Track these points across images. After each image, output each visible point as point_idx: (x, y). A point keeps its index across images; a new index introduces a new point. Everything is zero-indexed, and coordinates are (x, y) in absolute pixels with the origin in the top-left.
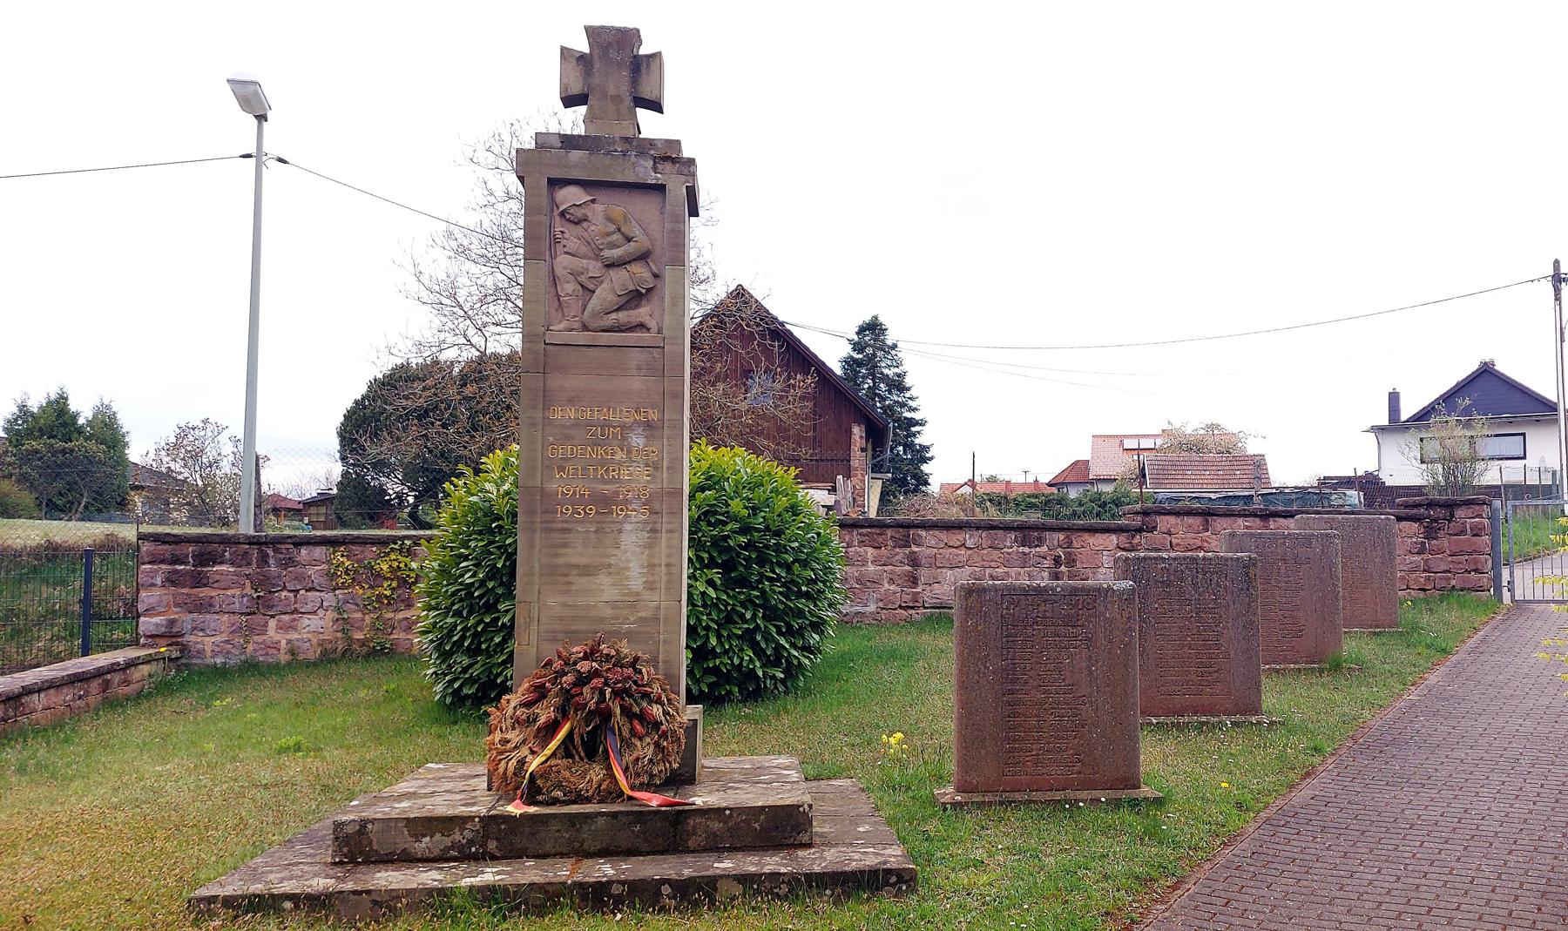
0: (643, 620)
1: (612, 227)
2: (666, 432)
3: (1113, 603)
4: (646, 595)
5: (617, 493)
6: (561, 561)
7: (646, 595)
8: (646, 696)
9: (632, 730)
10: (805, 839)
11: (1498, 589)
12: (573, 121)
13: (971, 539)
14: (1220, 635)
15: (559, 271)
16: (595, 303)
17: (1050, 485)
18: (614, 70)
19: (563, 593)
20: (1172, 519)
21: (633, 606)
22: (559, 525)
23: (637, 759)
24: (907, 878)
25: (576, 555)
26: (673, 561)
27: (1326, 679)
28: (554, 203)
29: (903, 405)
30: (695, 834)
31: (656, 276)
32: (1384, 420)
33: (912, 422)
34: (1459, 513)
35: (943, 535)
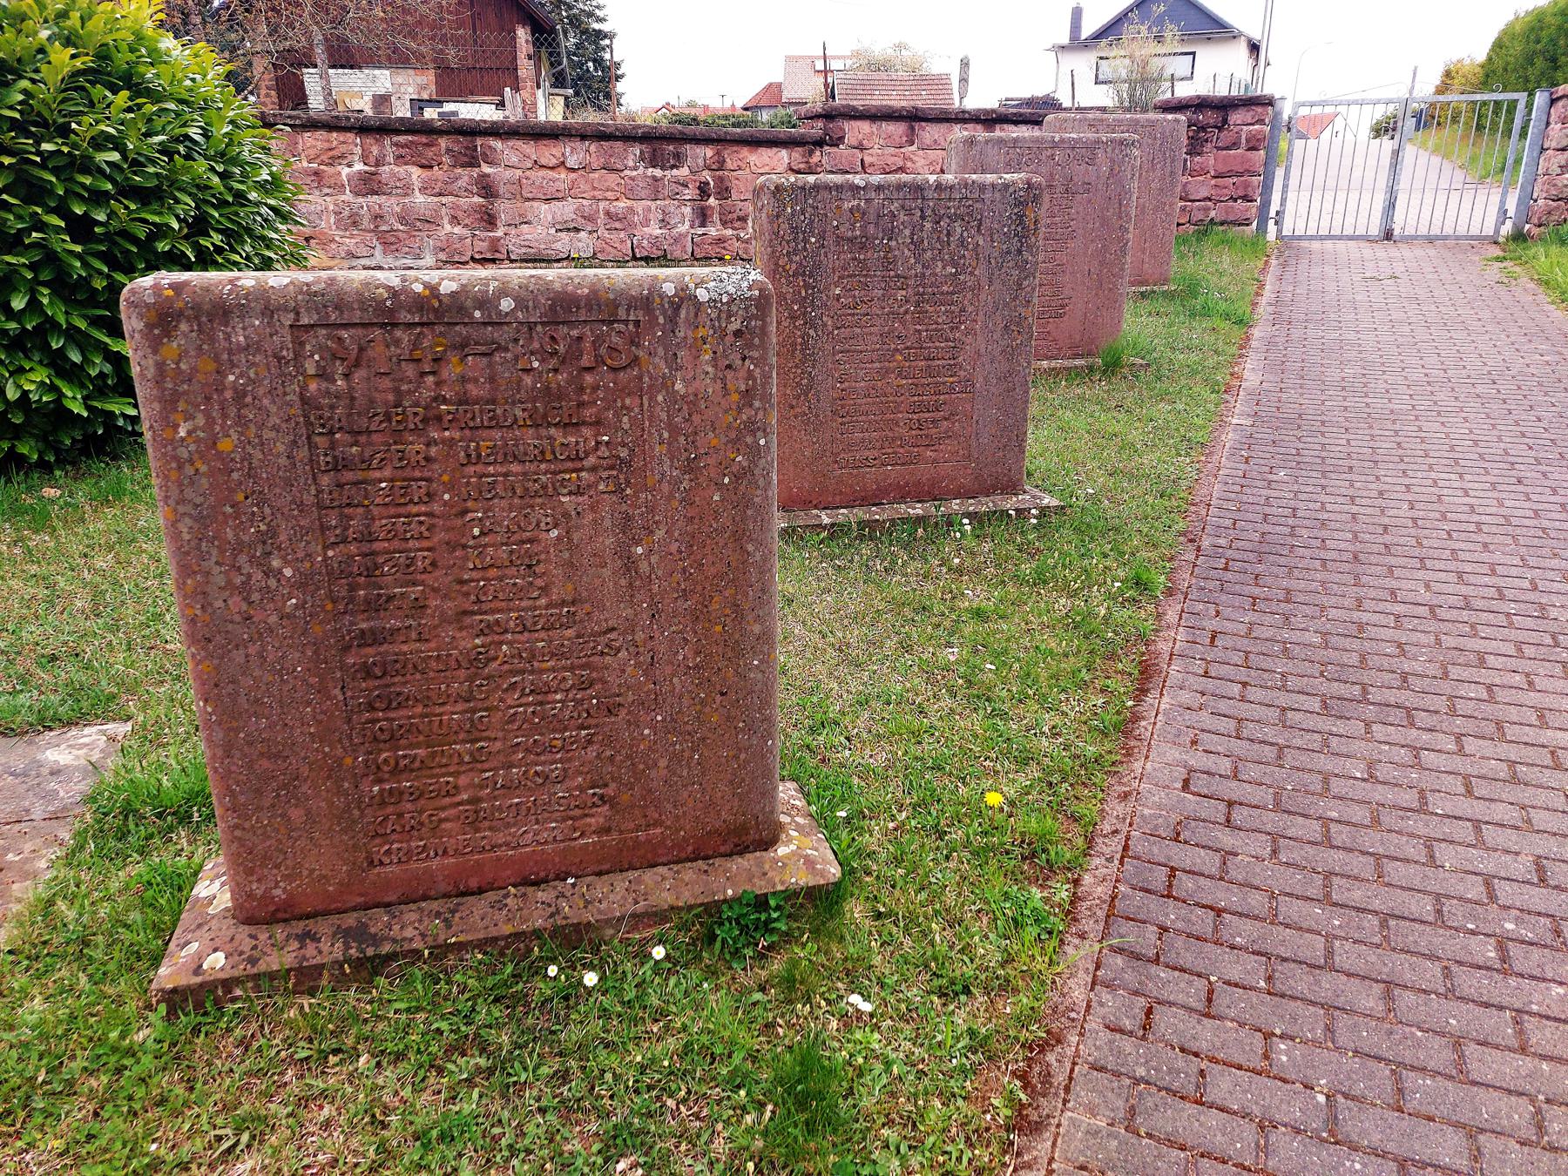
3: (696, 348)
11: (1262, 228)
13: (575, 154)
14: (957, 347)
17: (746, 109)
20: (865, 126)
27: (1100, 388)
29: (590, 15)
32: (1065, 40)
33: (600, 35)
34: (1236, 117)
35: (528, 148)
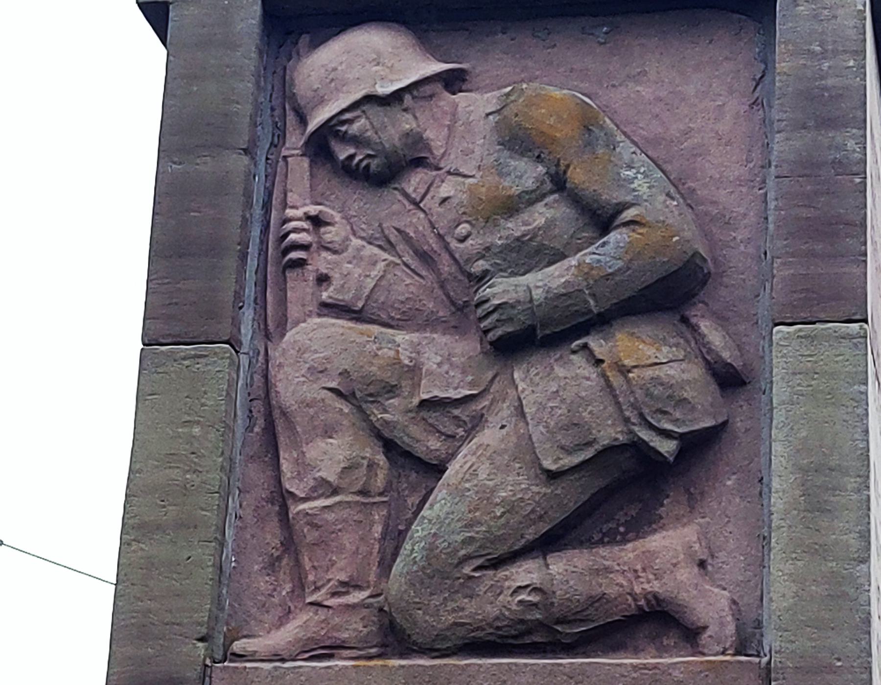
1: (527, 174)
15: (293, 387)
28: (284, 102)
31: (730, 380)
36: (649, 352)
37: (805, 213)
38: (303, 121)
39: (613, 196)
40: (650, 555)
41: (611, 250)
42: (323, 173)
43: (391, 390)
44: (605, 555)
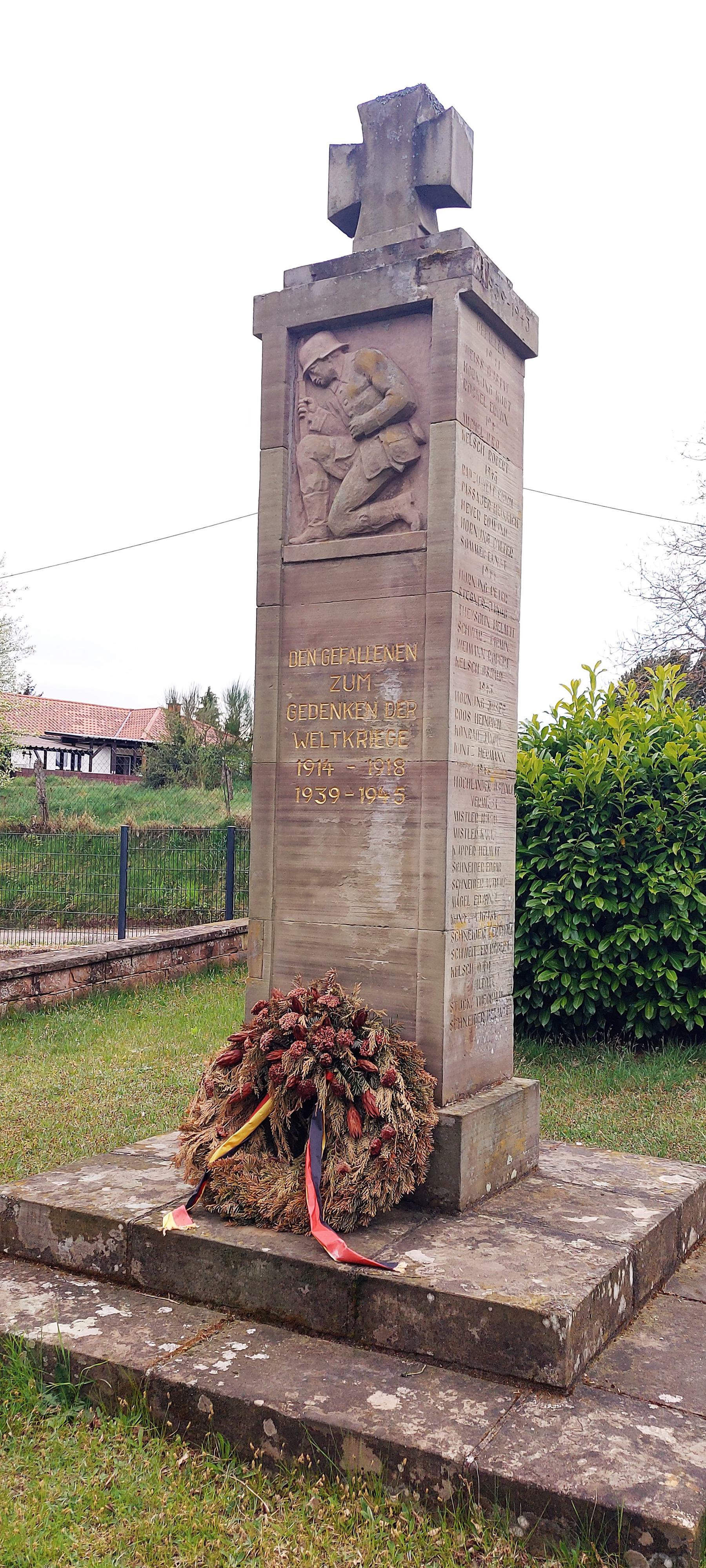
0: (394, 955)
2: (427, 676)
4: (401, 919)
5: (365, 769)
6: (299, 864)
7: (401, 919)
8: (369, 1075)
9: (345, 1124)
10: (552, 1377)
12: (340, 245)
15: (302, 459)
16: (341, 495)
18: (403, 159)
19: (303, 908)
21: (384, 932)
22: (298, 815)
23: (343, 1172)
24: (672, 1544)
25: (317, 857)
26: (434, 870)
30: (383, 1320)
36: (395, 437)
37: (439, 384)
38: (302, 369)
39: (385, 386)
40: (397, 502)
41: (383, 406)
42: (310, 386)
43: (328, 457)
44: (385, 503)
